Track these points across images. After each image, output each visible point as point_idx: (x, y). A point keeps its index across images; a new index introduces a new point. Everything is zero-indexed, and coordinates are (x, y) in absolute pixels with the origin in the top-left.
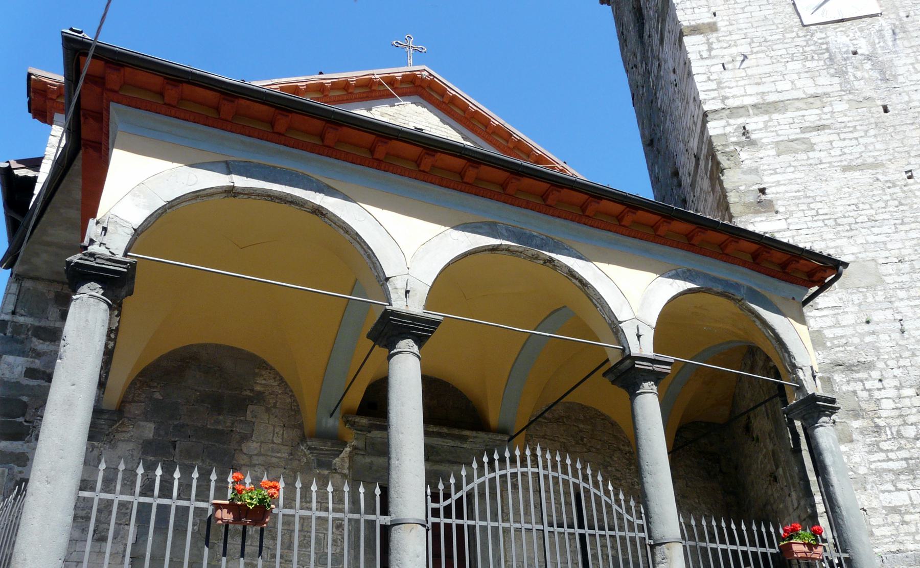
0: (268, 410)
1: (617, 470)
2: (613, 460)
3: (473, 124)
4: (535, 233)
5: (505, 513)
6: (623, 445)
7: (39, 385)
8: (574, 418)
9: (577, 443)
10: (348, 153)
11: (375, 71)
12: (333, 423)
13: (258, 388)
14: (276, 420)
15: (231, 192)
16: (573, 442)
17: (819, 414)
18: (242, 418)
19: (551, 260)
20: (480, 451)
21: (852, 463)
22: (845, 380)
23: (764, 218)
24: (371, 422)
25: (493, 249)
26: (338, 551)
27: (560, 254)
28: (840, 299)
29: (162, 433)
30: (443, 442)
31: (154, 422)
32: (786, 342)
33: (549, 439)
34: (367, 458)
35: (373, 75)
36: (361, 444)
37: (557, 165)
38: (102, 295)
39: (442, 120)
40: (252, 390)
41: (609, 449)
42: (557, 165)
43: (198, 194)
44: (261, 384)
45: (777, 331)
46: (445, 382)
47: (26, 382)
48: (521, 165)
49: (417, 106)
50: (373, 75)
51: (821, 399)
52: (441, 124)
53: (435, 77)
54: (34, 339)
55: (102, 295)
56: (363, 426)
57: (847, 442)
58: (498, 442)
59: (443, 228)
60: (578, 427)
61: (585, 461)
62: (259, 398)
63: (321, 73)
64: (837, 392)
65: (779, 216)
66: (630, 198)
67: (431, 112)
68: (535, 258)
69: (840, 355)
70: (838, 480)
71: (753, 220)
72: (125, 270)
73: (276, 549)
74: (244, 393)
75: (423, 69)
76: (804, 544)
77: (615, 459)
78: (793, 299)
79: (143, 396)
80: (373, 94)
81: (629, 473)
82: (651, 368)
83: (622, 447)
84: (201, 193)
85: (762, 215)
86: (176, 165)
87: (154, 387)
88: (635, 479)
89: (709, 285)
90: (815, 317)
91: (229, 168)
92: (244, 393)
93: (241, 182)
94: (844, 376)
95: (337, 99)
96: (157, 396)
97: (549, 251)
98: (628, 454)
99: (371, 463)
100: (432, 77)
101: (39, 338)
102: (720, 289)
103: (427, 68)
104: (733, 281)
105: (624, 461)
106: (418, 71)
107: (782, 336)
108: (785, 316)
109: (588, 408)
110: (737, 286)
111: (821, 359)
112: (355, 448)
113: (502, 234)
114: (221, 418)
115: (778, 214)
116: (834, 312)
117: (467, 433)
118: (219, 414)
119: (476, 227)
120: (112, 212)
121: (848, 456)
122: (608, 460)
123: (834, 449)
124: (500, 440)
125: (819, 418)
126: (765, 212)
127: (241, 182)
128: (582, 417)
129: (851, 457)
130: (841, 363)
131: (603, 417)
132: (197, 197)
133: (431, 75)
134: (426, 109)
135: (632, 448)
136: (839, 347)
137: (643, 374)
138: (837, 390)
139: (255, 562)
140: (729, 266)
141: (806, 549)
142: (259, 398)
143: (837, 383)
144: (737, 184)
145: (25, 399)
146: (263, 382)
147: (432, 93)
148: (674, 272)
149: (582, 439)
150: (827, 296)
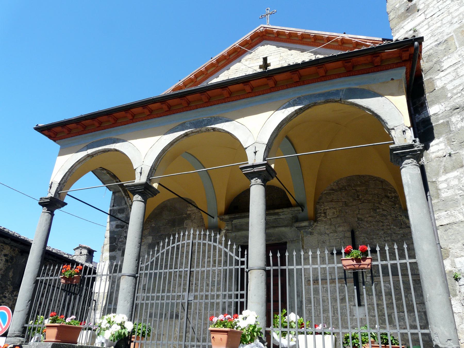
0: (192, 221)
1: (383, 210)
2: (381, 204)
3: (292, 39)
4: (204, 119)
5: (305, 249)
6: (390, 193)
7: (119, 230)
8: (353, 185)
9: (355, 200)
10: (121, 122)
11: (235, 43)
12: (216, 220)
13: (188, 212)
14: (195, 224)
15: (88, 156)
16: (352, 200)
17: (402, 159)
18: (182, 227)
19: (214, 129)
20: (290, 218)
21: (462, 184)
22: (460, 119)
23: (410, 20)
24: (229, 217)
25: (186, 135)
26: (219, 279)
27: (216, 124)
28: (459, 55)
29: (154, 239)
30: (269, 218)
31: (152, 236)
32: (379, 115)
33: (335, 202)
34: (232, 233)
35: (235, 45)
36: (230, 228)
37: (338, 37)
38: (47, 210)
39: (278, 47)
40: (186, 214)
41: (378, 198)
42: (338, 37)
43: (79, 161)
44: (190, 210)
45: (372, 110)
46: (269, 185)
47: (118, 230)
48: (179, 93)
49: (264, 46)
50: (235, 45)
51: (398, 148)
52: (277, 49)
53: (266, 28)
54: (118, 214)
55: (47, 210)
56: (227, 219)
57: (458, 168)
58: (296, 211)
59: (160, 136)
60: (356, 190)
61: (359, 210)
62: (189, 216)
63: (212, 58)
64: (453, 131)
65: (420, 12)
66: (238, 79)
67: (271, 45)
68: (208, 130)
69: (457, 101)
70: (411, 206)
71: (403, 25)
72: (49, 200)
73: (193, 281)
74: (183, 216)
75: (260, 28)
76: (352, 259)
77: (383, 203)
78: (392, 79)
79: (149, 226)
80: (240, 53)
81: (393, 210)
82: (252, 171)
83: (389, 195)
84: (80, 161)
85: (409, 18)
86: (73, 154)
87: (152, 222)
88: (399, 213)
89: (313, 100)
90: (440, 78)
91: (88, 147)
92: (183, 216)
93: (90, 151)
94: (459, 116)
95: (223, 65)
96: (153, 225)
97: (211, 125)
98: (393, 198)
99: (236, 236)
100: (265, 29)
101: (120, 213)
102: (322, 99)
103: (262, 25)
104: (334, 90)
105: (390, 203)
106: (258, 29)
107: (376, 112)
108: (381, 96)
109: (363, 176)
110: (337, 93)
111: (443, 109)
112: (227, 230)
113: (187, 127)
114: (174, 228)
115: (420, 12)
116: (455, 68)
117: (277, 211)
118: (174, 227)
119: (176, 129)
120: (54, 180)
121: (459, 179)
122: (378, 205)
123: (410, 182)
124: (297, 210)
125: (403, 162)
126: (411, 15)
127: (90, 151)
128: (359, 183)
129: (462, 179)
130: (458, 106)
131: (375, 179)
132: (80, 163)
133: (264, 28)
134: (269, 45)
135: (397, 193)
136: (457, 94)
137: (249, 175)
138: (454, 129)
139: (185, 288)
140: (328, 82)
141: (355, 262)
142: (189, 216)
143: (454, 123)
144: (394, 5)
145: (115, 236)
146: (190, 209)
147: (270, 36)
148: (287, 103)
149: (358, 196)
150: (450, 58)
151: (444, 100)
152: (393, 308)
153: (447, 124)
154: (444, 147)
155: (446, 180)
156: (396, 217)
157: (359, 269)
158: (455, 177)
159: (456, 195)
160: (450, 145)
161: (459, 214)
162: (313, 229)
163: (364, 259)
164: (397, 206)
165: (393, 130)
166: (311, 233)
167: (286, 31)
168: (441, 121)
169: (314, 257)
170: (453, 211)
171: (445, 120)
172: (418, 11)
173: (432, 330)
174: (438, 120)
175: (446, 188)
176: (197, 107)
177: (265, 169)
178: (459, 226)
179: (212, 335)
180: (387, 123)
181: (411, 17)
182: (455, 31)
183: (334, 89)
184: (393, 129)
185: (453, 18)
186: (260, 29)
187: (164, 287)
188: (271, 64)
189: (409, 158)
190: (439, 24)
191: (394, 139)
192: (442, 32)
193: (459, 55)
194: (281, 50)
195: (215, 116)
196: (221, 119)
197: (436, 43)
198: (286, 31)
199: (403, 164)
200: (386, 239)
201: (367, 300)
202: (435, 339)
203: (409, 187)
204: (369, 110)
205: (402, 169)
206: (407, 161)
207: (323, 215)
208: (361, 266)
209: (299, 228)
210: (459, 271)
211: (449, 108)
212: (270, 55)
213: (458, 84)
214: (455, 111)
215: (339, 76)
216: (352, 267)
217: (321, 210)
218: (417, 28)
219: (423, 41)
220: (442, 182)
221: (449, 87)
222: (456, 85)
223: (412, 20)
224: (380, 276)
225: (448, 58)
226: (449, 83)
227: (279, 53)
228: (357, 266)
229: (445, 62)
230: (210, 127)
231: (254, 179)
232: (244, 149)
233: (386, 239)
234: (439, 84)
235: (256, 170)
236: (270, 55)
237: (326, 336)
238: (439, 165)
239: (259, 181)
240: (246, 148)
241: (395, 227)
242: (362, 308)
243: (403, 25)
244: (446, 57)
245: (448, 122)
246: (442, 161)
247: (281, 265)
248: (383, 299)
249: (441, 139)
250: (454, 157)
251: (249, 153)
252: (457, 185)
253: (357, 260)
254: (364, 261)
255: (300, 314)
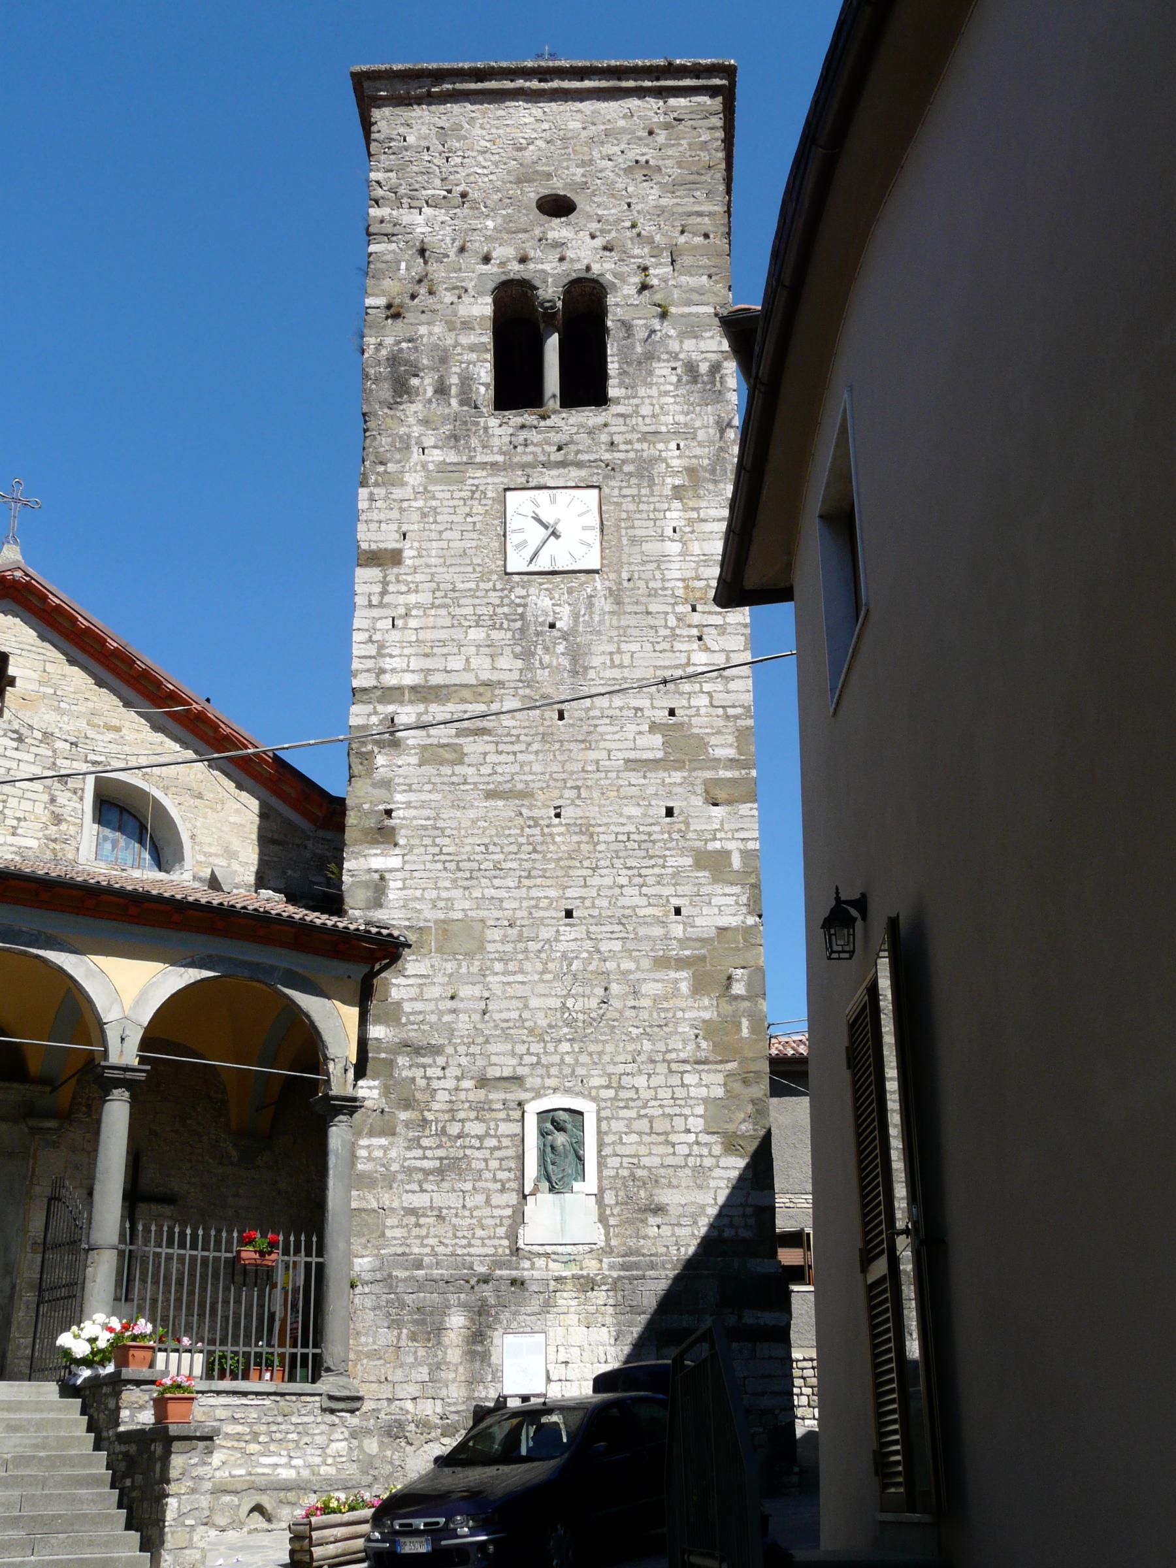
4: (24, 929)
39: (42, 637)
49: (6, 615)
52: (38, 642)
53: (32, 578)
65: (397, 851)
69: (412, 1034)
71: (367, 852)
82: (122, 1076)
90: (398, 986)
100: (28, 579)
107: (317, 1024)
130: (410, 1043)
133: (27, 575)
136: (413, 1024)
141: (257, 1256)
148: (189, 960)
151: (394, 1024)
152: (181, 1309)
153: (391, 1063)
154: (376, 1096)
155: (368, 1147)
157: (261, 1265)
158: (381, 1147)
159: (376, 1172)
160: (386, 1097)
161: (373, 1200)
162: (60, 1137)
163: (270, 1253)
164: (222, 1120)
165: (332, 1062)
166: (56, 1145)
167: (80, 618)
168: (383, 1055)
169: (218, 1242)
170: (367, 1194)
171: (389, 1056)
172: (396, 845)
173: (327, 1350)
174: (379, 1050)
175: (365, 1158)
176: (16, 902)
177: (143, 1079)
178: (369, 1215)
179: (131, 1353)
180: (327, 1048)
181: (382, 846)
182: (436, 922)
184: (333, 1060)
185: (439, 898)
188: (18, 682)
189: (344, 1114)
190: (418, 893)
191: (332, 1076)
192: (419, 911)
193: (432, 966)
194: (48, 654)
195: (50, 931)
196: (59, 944)
197: (407, 923)
198: (80, 618)
199: (336, 1119)
200: (193, 1180)
201: (139, 1289)
203: (337, 1158)
206: (341, 1117)
207: (84, 1109)
208: (265, 1262)
209: (33, 1131)
210: (358, 1275)
211: (398, 1041)
213: (418, 1010)
214: (405, 1049)
215: (283, 945)
216: (253, 1262)
217: (81, 1097)
218: (387, 876)
219: (345, 799)
220: (363, 1147)
221: (407, 1006)
222: (416, 1009)
223: (382, 854)
225: (417, 960)
226: (407, 1000)
227: (42, 657)
228: (259, 1262)
229: (411, 963)
231: (120, 1090)
232: (101, 1025)
233: (193, 1180)
234: (395, 994)
235: (129, 1075)
237: (196, 1355)
238: (364, 1121)
239: (127, 1094)
240: (106, 1024)
241: (211, 1161)
242: (128, 1304)
243: (367, 852)
244: (414, 957)
245: (392, 1060)
246: (369, 1117)
249: (376, 1083)
250: (386, 1117)
251: (112, 1036)
252: (380, 1158)
253: (262, 1254)
254: (269, 1255)
255: (152, 1320)
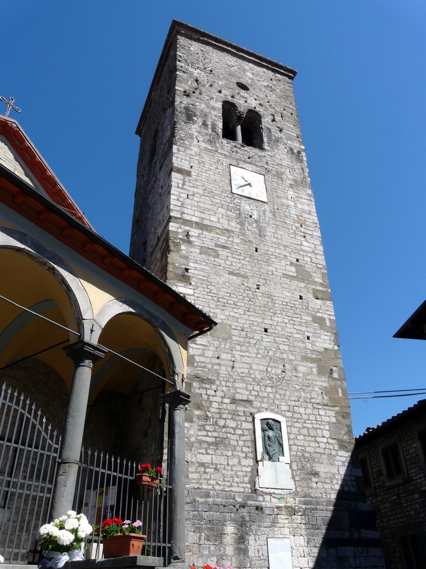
27: (60, 267)
49: (2, 142)
52: (14, 160)
53: (20, 130)
69: (199, 372)
70: (179, 443)
71: (177, 284)
77: (56, 402)
82: (93, 352)
102: (147, 317)
107: (172, 353)
110: (157, 318)
133: (18, 128)
136: (200, 367)
144: (175, 262)
148: (124, 299)
156: (61, 421)
183: (156, 313)
186: (13, 124)
187: (40, 463)
194: (17, 167)
202: (176, 552)
204: (169, 349)
205: (177, 410)
212: (5, 160)
214: (196, 379)
222: (201, 360)
223: (184, 287)
224: (33, 478)
230: (52, 264)
236: (5, 160)
247: (44, 454)
248: (28, 504)
